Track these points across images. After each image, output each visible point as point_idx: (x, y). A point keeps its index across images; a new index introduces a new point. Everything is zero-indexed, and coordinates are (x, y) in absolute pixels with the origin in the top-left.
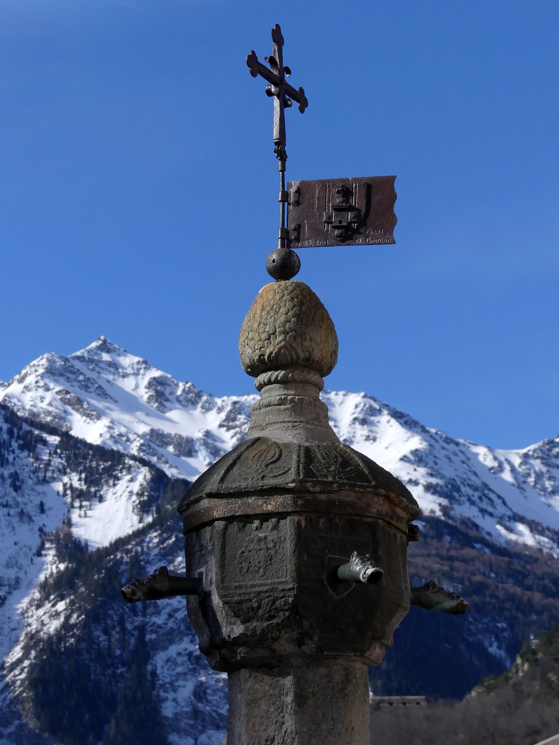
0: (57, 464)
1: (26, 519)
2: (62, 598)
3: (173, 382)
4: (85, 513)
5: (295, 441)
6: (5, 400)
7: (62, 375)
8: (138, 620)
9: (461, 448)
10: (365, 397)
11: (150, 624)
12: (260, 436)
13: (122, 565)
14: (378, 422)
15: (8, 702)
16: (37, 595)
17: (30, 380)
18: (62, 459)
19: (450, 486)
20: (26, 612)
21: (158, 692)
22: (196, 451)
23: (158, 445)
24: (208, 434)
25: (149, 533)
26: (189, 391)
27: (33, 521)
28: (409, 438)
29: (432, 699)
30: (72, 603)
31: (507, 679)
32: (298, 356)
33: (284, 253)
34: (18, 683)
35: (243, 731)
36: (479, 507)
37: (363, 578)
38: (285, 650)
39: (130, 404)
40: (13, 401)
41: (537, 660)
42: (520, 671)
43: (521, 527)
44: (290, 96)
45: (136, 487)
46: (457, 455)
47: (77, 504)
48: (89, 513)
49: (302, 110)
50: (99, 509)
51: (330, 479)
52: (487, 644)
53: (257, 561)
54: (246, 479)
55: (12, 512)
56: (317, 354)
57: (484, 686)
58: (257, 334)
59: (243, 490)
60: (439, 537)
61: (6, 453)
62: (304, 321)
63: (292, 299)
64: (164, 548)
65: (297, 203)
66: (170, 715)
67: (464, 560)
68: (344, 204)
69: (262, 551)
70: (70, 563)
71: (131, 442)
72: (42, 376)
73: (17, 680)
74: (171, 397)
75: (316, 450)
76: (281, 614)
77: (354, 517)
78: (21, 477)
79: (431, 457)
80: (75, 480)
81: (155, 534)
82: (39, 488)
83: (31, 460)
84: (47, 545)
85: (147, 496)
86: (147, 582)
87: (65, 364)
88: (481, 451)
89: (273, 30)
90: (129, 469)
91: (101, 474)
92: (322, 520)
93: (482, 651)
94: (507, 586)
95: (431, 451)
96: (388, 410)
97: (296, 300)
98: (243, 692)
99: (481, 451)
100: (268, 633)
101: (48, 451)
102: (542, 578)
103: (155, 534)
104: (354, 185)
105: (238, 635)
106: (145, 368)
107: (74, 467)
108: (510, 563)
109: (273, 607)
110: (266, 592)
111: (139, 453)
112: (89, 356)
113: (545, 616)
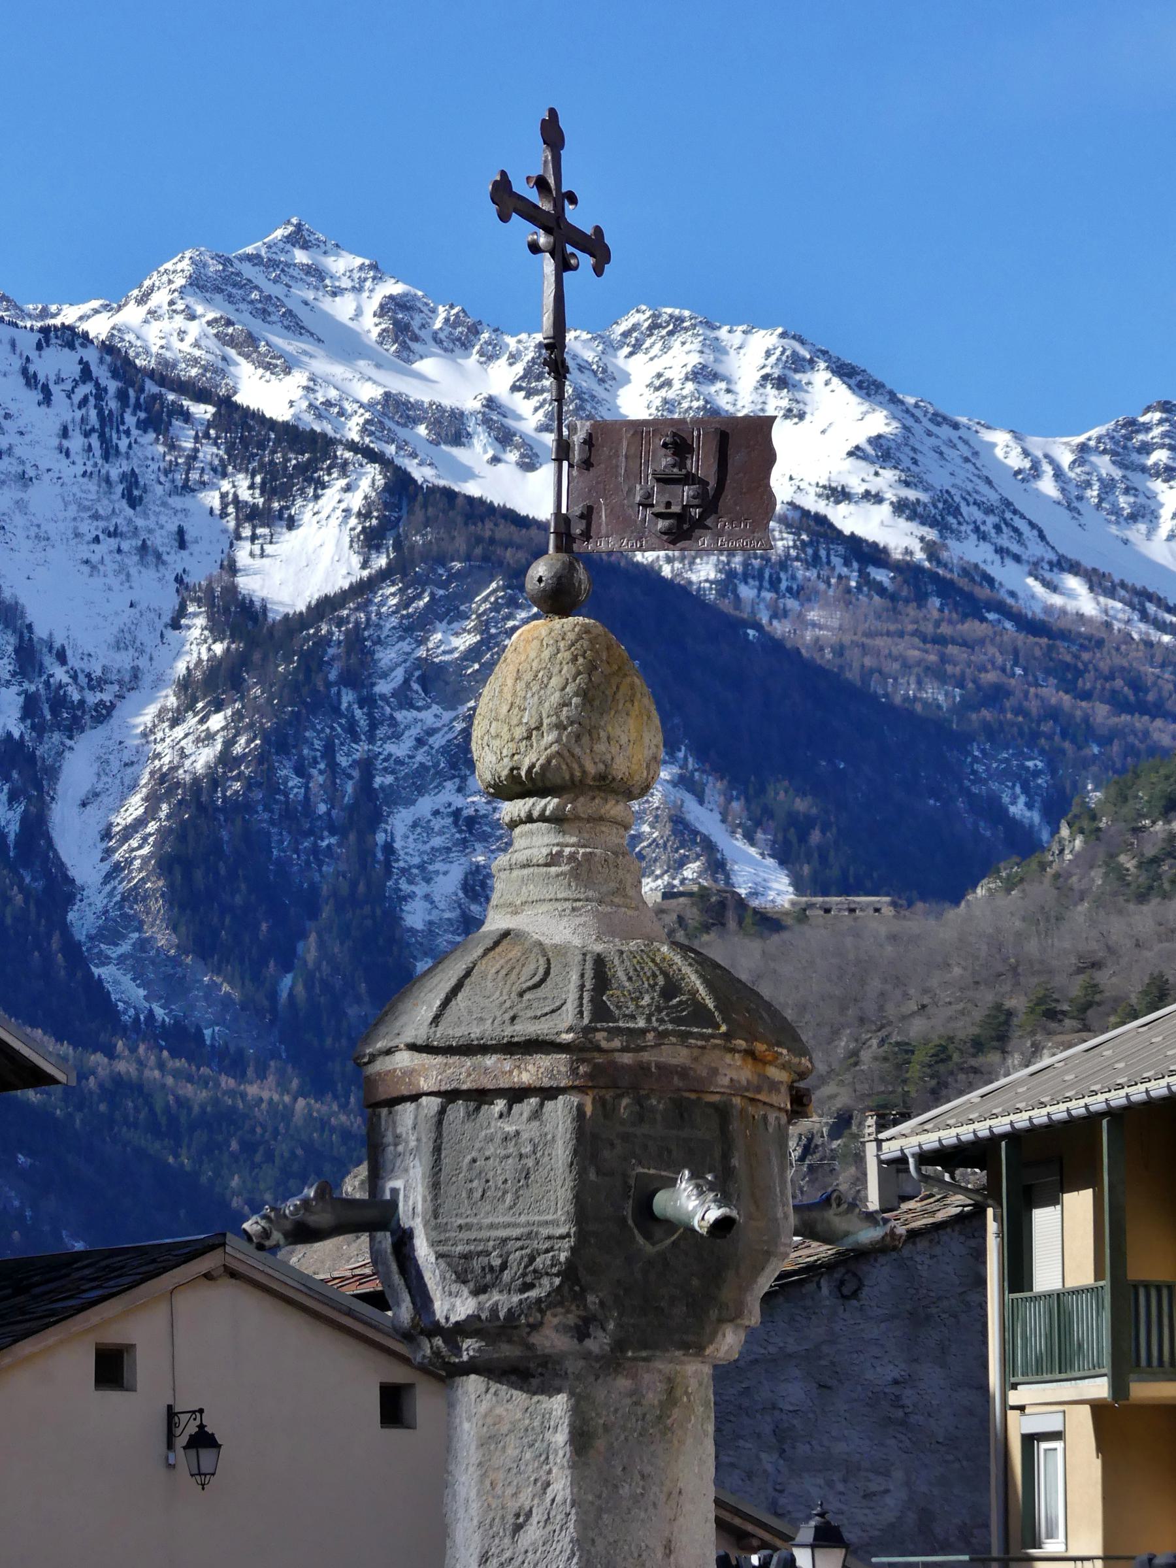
0: (209, 457)
1: (151, 559)
2: (219, 707)
3: (427, 304)
4: (262, 549)
5: (577, 942)
6: (113, 335)
7: (220, 290)
8: (361, 749)
9: (962, 432)
10: (783, 335)
11: (382, 757)
12: (511, 926)
13: (330, 646)
14: (809, 383)
15: (118, 898)
16: (172, 702)
17: (160, 299)
18: (219, 449)
19: (940, 505)
20: (152, 732)
21: (397, 883)
22: (469, 435)
23: (398, 423)
24: (491, 403)
25: (381, 588)
26: (457, 323)
27: (164, 563)
28: (865, 413)
29: (903, 902)
30: (238, 716)
31: (1043, 866)
32: (584, 772)
33: (559, 565)
34: (137, 863)
35: (473, 1494)
36: (995, 544)
37: (701, 1227)
38: (553, 1346)
39: (346, 346)
40: (127, 338)
41: (1099, 829)
42: (1067, 851)
43: (1073, 583)
44: (573, 246)
45: (356, 501)
46: (954, 446)
47: (246, 532)
48: (269, 549)
49: (598, 271)
50: (289, 542)
51: (641, 1023)
52: (1006, 799)
53: (500, 1180)
54: (481, 1020)
55: (126, 546)
56: (620, 768)
57: (1000, 878)
58: (506, 728)
59: (475, 1043)
60: (920, 599)
61: (115, 436)
62: (597, 703)
63: (575, 659)
64: (409, 616)
65: (587, 464)
66: (419, 926)
67: (965, 644)
68: (675, 470)
69: (510, 1161)
70: (233, 642)
71: (349, 417)
72: (182, 291)
73: (135, 858)
74: (422, 334)
75: (616, 962)
76: (545, 1281)
77: (686, 1094)
78: (142, 482)
79: (907, 450)
80: (243, 487)
81: (393, 589)
82: (176, 502)
83: (161, 449)
84: (192, 608)
85: (377, 518)
86: (292, 1213)
87: (224, 270)
88: (1000, 439)
89: (544, 120)
90: (344, 467)
91: (291, 477)
92: (625, 1101)
93: (995, 812)
94: (1044, 691)
95: (906, 438)
96: (826, 361)
97: (581, 660)
98: (474, 1420)
99: (1000, 439)
100: (519, 1316)
101: (193, 433)
102: (1111, 677)
103: (393, 589)
104: (695, 433)
105: (463, 1317)
106: (374, 278)
107: (241, 464)
108: (1050, 648)
109: (531, 1268)
110: (517, 1239)
111: (362, 437)
112: (270, 255)
113: (1116, 747)
